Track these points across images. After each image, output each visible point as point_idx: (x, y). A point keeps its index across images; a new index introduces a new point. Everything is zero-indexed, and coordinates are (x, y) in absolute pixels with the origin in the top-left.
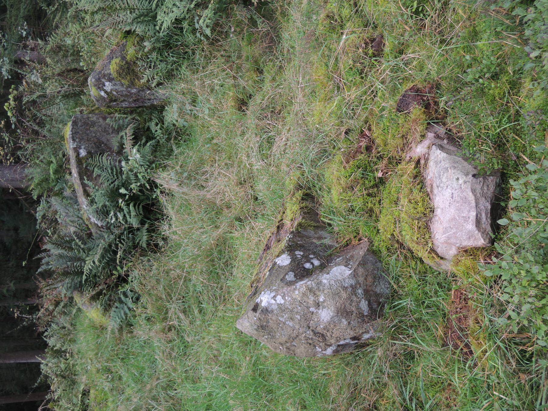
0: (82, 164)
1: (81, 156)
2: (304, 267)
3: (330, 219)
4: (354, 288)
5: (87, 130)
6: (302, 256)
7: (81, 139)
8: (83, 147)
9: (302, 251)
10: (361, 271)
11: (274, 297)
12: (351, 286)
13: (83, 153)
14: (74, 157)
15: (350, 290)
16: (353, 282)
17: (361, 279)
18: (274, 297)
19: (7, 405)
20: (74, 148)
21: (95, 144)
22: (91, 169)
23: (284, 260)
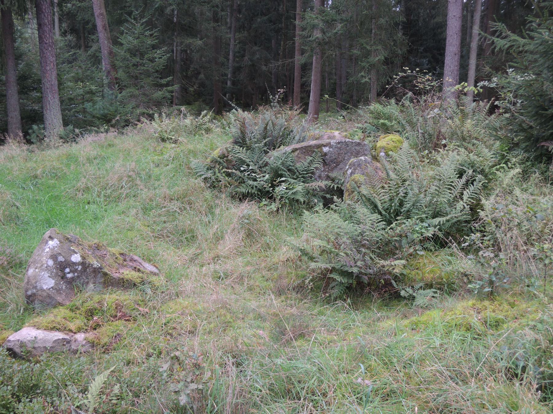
0: (317, 148)
1: (323, 148)
2: (67, 268)
3: (198, 334)
4: (35, 287)
5: (352, 153)
6: (77, 269)
7: (340, 148)
8: (331, 149)
9: (81, 270)
10: (45, 294)
11: (49, 248)
12: (36, 287)
13: (326, 149)
14: (323, 143)
15: (35, 285)
16: (38, 288)
17: (40, 293)
18: (49, 248)
19: (443, 26)
20: (330, 143)
21: (335, 159)
22: (313, 155)
23: (76, 258)
